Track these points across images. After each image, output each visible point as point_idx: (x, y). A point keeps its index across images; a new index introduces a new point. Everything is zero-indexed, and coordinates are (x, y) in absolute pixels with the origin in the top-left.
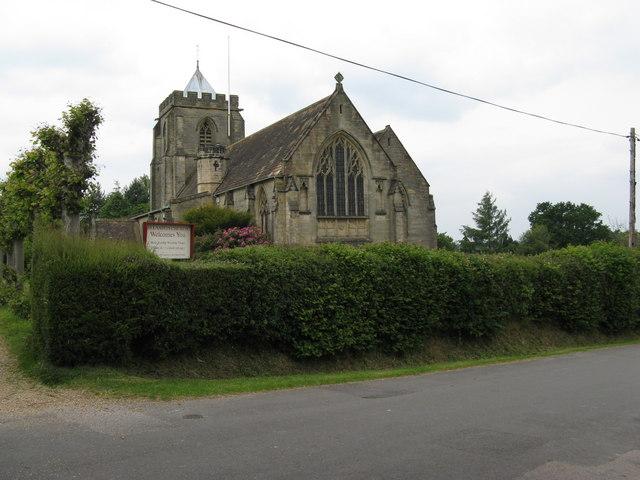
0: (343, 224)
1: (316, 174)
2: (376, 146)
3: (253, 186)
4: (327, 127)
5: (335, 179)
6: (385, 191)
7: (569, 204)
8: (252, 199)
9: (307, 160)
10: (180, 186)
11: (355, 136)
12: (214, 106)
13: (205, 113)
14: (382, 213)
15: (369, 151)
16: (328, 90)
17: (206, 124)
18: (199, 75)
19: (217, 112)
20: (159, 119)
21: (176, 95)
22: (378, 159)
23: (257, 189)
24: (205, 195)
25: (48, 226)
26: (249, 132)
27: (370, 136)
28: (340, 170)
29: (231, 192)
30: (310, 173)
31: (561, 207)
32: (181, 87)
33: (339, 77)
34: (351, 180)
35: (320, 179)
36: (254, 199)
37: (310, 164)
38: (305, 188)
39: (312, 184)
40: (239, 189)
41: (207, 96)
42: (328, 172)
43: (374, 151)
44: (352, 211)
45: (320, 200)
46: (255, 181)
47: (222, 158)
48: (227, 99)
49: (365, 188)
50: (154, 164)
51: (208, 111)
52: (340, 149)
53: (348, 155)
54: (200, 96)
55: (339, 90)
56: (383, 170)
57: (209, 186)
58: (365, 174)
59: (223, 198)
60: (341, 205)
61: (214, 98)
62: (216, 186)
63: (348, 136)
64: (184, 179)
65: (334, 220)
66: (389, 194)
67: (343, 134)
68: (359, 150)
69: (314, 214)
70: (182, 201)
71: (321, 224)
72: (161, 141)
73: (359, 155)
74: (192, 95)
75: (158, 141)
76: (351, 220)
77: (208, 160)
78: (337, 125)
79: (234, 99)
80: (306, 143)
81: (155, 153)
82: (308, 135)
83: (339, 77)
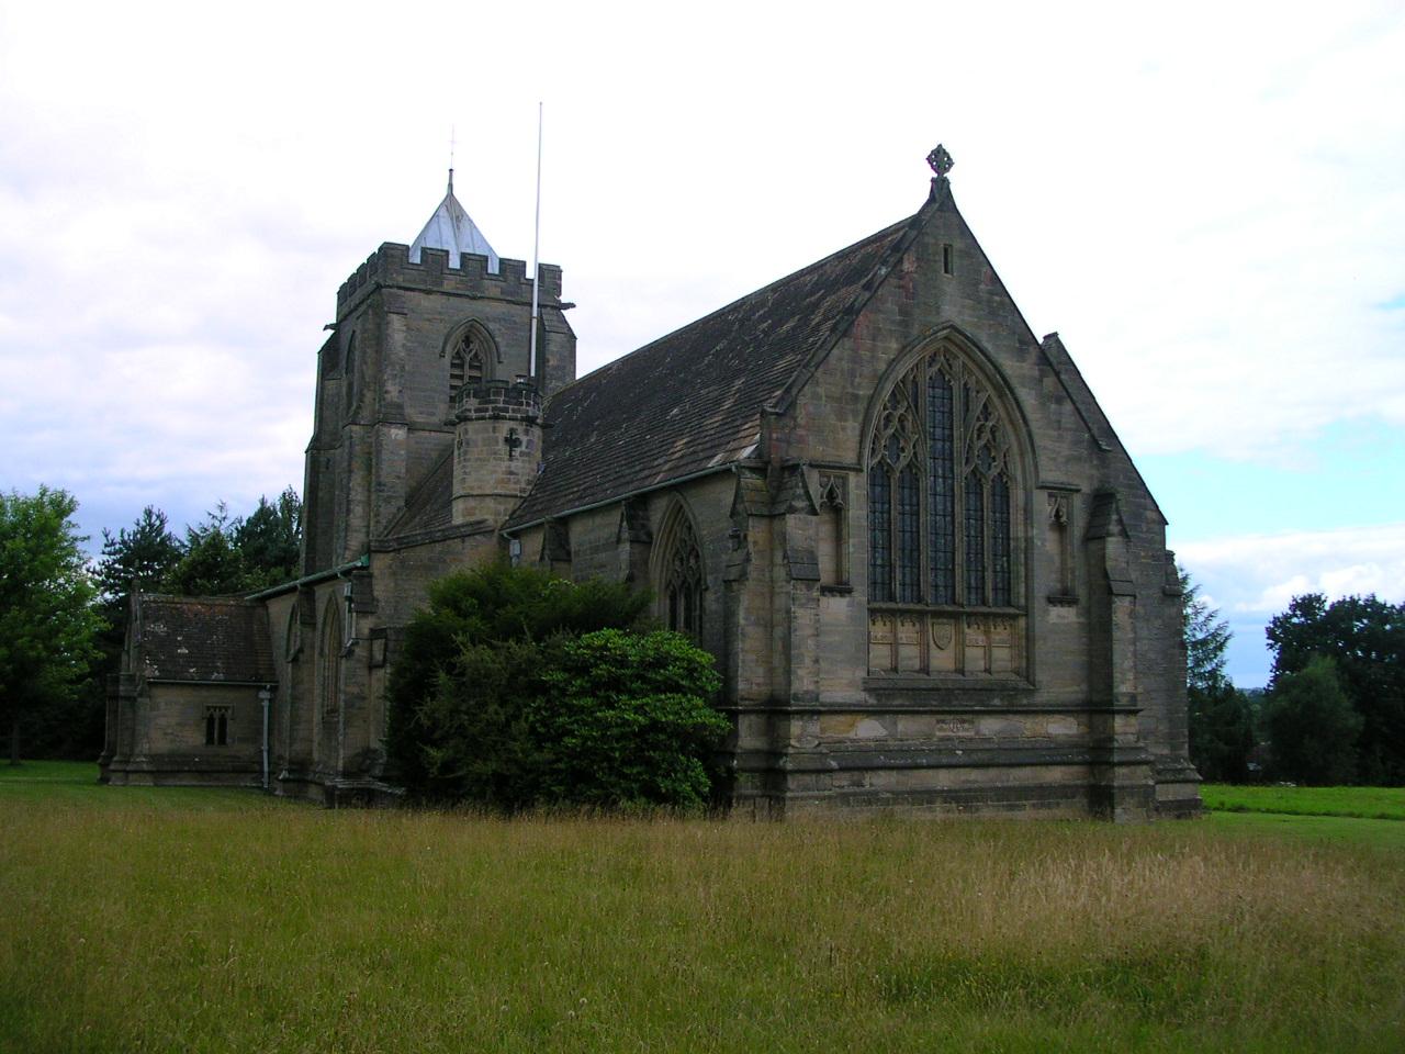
1: (868, 462)
2: (1049, 382)
3: (642, 501)
4: (904, 311)
5: (926, 482)
7: (1372, 602)
8: (643, 540)
9: (841, 417)
10: (388, 511)
11: (988, 346)
12: (495, 292)
13: (469, 309)
14: (1063, 598)
15: (1028, 397)
16: (907, 199)
17: (467, 341)
18: (451, 208)
19: (501, 308)
21: (389, 255)
22: (1059, 426)
24: (476, 529)
26: (589, 360)
27: (1033, 354)
29: (564, 521)
30: (849, 457)
31: (1349, 609)
32: (406, 237)
33: (940, 160)
36: (648, 543)
37: (852, 427)
38: (834, 508)
39: (857, 489)
40: (591, 512)
41: (475, 263)
43: (1045, 400)
46: (657, 481)
47: (530, 421)
48: (531, 273)
50: (318, 454)
51: (479, 305)
53: (967, 405)
54: (454, 263)
55: (941, 194)
56: (1069, 460)
57: (490, 503)
58: (1016, 470)
59: (535, 543)
61: (494, 268)
62: (511, 505)
63: (969, 345)
64: (401, 490)
67: (958, 341)
68: (1001, 396)
69: (861, 594)
70: (405, 544)
71: (880, 630)
72: (338, 386)
73: (999, 410)
74: (434, 259)
75: (331, 385)
77: (489, 424)
78: (938, 310)
80: (840, 355)
82: (845, 334)
83: (940, 160)
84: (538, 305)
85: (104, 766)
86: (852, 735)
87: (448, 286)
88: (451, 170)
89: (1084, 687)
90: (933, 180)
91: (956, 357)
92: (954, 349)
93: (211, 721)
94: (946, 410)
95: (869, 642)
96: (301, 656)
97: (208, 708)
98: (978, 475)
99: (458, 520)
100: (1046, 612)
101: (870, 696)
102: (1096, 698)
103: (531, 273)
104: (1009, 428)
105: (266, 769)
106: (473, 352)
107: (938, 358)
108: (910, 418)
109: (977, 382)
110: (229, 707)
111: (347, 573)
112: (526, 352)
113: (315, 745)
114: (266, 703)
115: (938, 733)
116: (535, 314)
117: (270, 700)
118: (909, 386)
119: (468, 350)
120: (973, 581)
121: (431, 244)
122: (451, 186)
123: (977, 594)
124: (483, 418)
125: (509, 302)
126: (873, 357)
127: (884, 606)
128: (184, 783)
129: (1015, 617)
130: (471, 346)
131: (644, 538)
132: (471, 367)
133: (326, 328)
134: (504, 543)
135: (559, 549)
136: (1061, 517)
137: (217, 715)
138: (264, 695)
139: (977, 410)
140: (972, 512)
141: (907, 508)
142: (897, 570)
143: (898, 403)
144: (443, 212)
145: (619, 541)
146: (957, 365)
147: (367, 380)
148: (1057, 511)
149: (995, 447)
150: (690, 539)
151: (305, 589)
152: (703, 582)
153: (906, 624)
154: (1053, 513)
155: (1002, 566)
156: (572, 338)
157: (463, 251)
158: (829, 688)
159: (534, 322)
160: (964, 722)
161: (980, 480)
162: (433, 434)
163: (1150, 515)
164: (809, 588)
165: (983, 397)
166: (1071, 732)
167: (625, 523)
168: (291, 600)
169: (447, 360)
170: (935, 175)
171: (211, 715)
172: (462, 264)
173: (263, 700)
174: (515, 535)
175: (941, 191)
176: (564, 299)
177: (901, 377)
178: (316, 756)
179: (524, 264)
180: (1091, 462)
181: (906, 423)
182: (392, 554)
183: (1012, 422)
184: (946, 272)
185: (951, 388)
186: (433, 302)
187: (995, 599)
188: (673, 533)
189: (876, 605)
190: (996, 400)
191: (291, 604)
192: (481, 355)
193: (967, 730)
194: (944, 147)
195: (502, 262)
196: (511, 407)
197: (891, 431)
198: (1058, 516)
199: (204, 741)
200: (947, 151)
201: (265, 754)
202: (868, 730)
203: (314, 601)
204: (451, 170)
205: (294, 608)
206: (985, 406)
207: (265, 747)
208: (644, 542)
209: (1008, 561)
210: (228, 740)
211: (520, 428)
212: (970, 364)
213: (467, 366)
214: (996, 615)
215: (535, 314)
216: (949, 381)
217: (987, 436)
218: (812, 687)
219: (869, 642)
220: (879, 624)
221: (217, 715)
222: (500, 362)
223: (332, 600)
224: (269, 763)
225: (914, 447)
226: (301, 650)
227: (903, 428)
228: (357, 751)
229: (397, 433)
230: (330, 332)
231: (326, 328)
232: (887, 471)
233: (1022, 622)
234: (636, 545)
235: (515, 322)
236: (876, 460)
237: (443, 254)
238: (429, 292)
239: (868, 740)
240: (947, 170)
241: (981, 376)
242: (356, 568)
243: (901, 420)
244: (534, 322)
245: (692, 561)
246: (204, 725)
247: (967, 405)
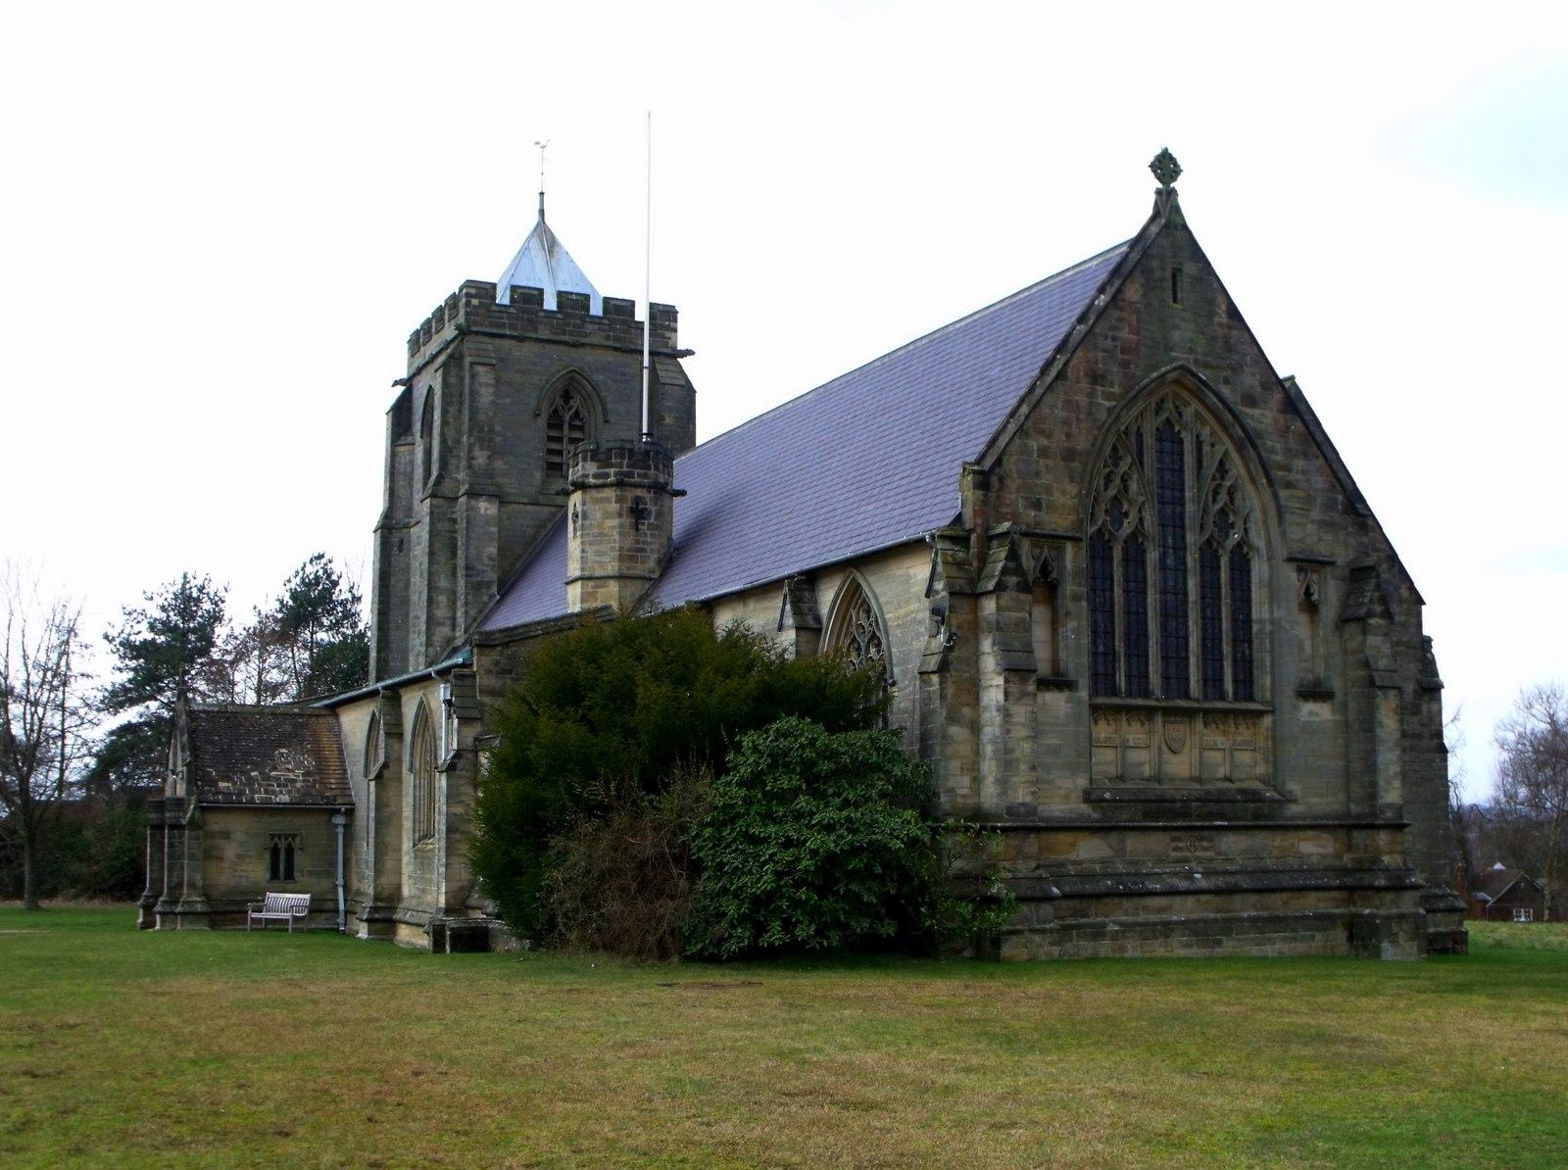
0: (1179, 730)
5: (1152, 555)
6: (1329, 612)
14: (1314, 692)
17: (567, 396)
18: (544, 237)
19: (610, 357)
20: (408, 383)
21: (478, 292)
23: (827, 596)
25: (1329, 951)
28: (1174, 525)
33: (1165, 167)
34: (1209, 563)
35: (1099, 550)
41: (574, 303)
42: (1128, 527)
44: (1212, 681)
45: (1100, 632)
48: (641, 314)
49: (1258, 595)
51: (574, 353)
52: (1169, 436)
53: (1199, 462)
55: (1167, 214)
58: (1257, 539)
60: (1174, 654)
61: (596, 309)
64: (492, 576)
65: (1149, 712)
66: (1343, 621)
68: (1240, 449)
71: (1103, 730)
73: (1236, 466)
74: (527, 298)
76: (1212, 716)
79: (664, 317)
81: (392, 493)
83: (1165, 167)
84: (651, 353)
85: (148, 909)
86: (1072, 856)
88: (542, 194)
89: (1341, 797)
90: (1159, 192)
91: (1187, 404)
92: (1185, 395)
93: (275, 852)
94: (1177, 467)
95: (1091, 746)
96: (385, 772)
97: (272, 837)
98: (1215, 544)
100: (1296, 709)
101: (1093, 809)
102: (1355, 809)
104: (1250, 488)
105: (342, 907)
106: (573, 410)
107: (1165, 406)
108: (1135, 477)
109: (1211, 434)
110: (296, 835)
112: (637, 404)
113: (405, 877)
114: (340, 830)
115: (1173, 854)
116: (646, 363)
117: (345, 826)
118: (1133, 439)
119: (566, 408)
120: (1210, 672)
121: (522, 281)
122: (542, 212)
123: (1214, 687)
124: (604, 486)
125: (616, 349)
126: (1091, 403)
127: (1108, 701)
128: (1270, 950)
129: (1260, 714)
130: (572, 402)
131: (812, 623)
132: (572, 427)
133: (396, 383)
136: (1312, 594)
137: (282, 845)
138: (340, 820)
139: (1210, 467)
140: (1208, 590)
141: (1132, 585)
142: (1122, 659)
143: (1121, 458)
144: (535, 244)
145: (781, 628)
146: (1188, 413)
147: (450, 444)
148: (1308, 588)
149: (1233, 511)
150: (871, 625)
151: (388, 693)
152: (888, 674)
153: (1133, 724)
154: (1303, 590)
155: (1243, 653)
156: (688, 392)
157: (563, 289)
158: (1045, 801)
159: (646, 373)
160: (1202, 839)
161: (1216, 551)
162: (528, 507)
163: (1405, 592)
164: (1024, 681)
165: (1219, 451)
166: (1325, 851)
167: (788, 607)
169: (542, 421)
170: (1160, 186)
171: (276, 845)
172: (559, 305)
173: (337, 826)
175: (1167, 206)
176: (681, 346)
177: (1123, 428)
178: (406, 891)
180: (322, 625)
181: (1130, 483)
182: (499, 648)
183: (1253, 481)
184: (1175, 301)
185: (1181, 442)
186: (527, 350)
187: (1235, 693)
188: (848, 618)
189: (1100, 700)
190: (1234, 455)
191: (371, 709)
192: (583, 412)
193: (1205, 849)
194: (1170, 151)
195: (606, 300)
196: (636, 471)
197: (1111, 492)
198: (1308, 593)
199: (268, 876)
200: (1174, 155)
201: (340, 891)
202: (1090, 850)
203: (400, 706)
204: (542, 194)
205: (374, 715)
206: (1221, 463)
207: (340, 881)
208: (811, 629)
209: (1250, 648)
210: (297, 874)
212: (1204, 413)
213: (566, 426)
214: (1237, 713)
215: (646, 363)
216: (1179, 432)
217: (1223, 498)
218: (1028, 799)
219: (1091, 746)
220: (1102, 723)
221: (282, 845)
222: (606, 421)
223: (422, 707)
224: (345, 901)
225: (1140, 511)
226: (385, 766)
227: (1126, 488)
228: (460, 884)
229: (486, 508)
230: (400, 389)
231: (396, 383)
232: (1109, 540)
233: (1267, 720)
234: (802, 633)
235: (624, 374)
236: (1096, 528)
237: (535, 292)
238: (521, 339)
239: (1093, 861)
240: (1174, 178)
241: (1217, 427)
242: (456, 666)
243: (1124, 480)
244: (646, 373)
245: (873, 650)
246: (267, 856)
247: (1199, 462)
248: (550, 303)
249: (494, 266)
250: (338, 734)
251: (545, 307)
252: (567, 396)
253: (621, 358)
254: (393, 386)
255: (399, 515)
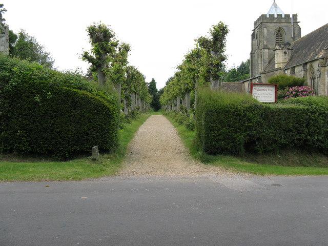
8: (306, 71)
12: (284, 21)
13: (278, 25)
17: (279, 31)
18: (275, 5)
20: (254, 30)
21: (263, 17)
24: (279, 69)
26: (304, 33)
29: (294, 67)
41: (280, 16)
48: (291, 16)
57: (282, 64)
62: (286, 64)
70: (267, 72)
72: (255, 42)
74: (272, 16)
75: (254, 42)
77: (281, 50)
79: (295, 16)
81: (252, 48)
87: (274, 21)
99: (276, 67)
103: (291, 16)
111: (257, 77)
121: (271, 13)
133: (21, 29)
134: (284, 71)
135: (293, 72)
156: (300, 28)
168: (248, 82)
174: (286, 70)
176: (298, 21)
179: (289, 15)
211: (287, 50)
229: (266, 50)
248: (276, 16)
249: (266, 12)
250: (244, 86)
251: (159, 90)
252: (279, 31)
253: (288, 24)
254: (93, 32)
255: (253, 51)
